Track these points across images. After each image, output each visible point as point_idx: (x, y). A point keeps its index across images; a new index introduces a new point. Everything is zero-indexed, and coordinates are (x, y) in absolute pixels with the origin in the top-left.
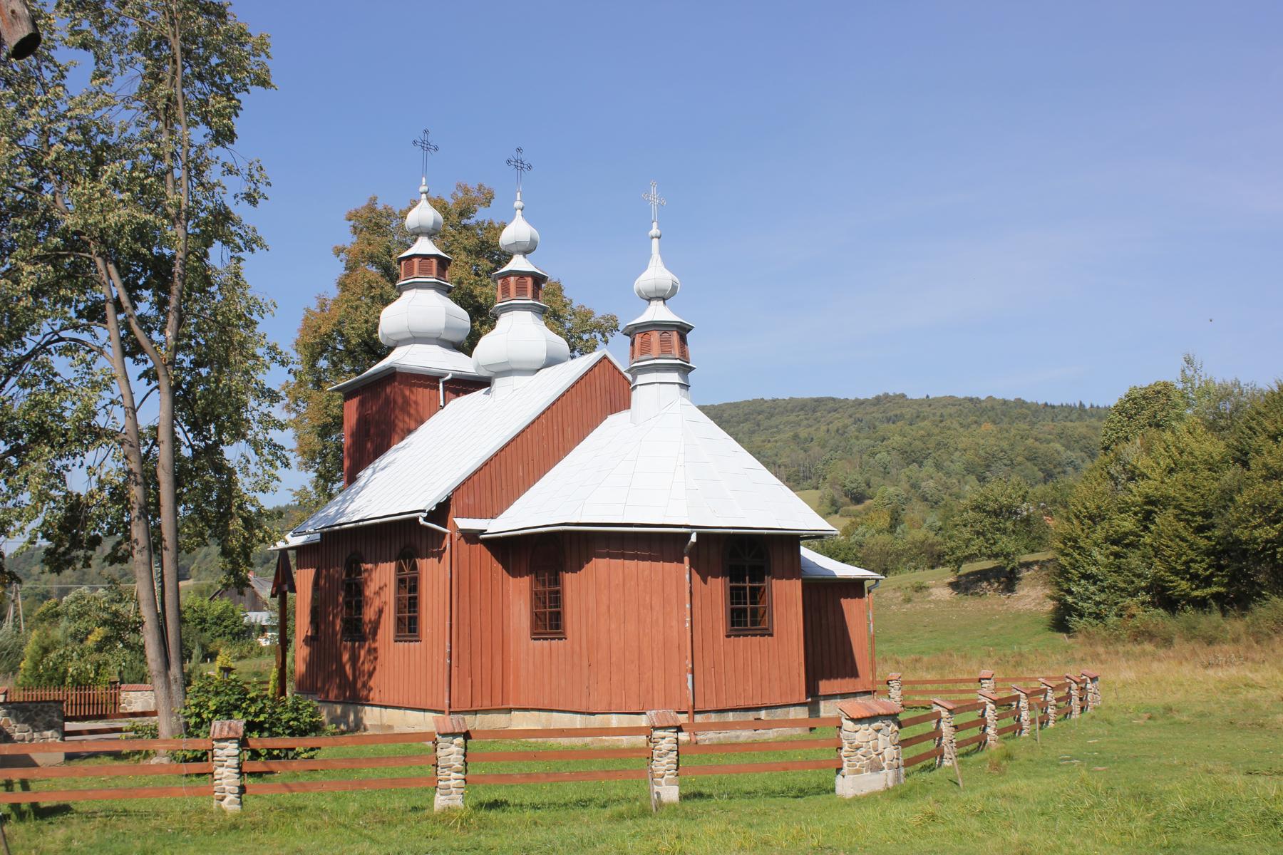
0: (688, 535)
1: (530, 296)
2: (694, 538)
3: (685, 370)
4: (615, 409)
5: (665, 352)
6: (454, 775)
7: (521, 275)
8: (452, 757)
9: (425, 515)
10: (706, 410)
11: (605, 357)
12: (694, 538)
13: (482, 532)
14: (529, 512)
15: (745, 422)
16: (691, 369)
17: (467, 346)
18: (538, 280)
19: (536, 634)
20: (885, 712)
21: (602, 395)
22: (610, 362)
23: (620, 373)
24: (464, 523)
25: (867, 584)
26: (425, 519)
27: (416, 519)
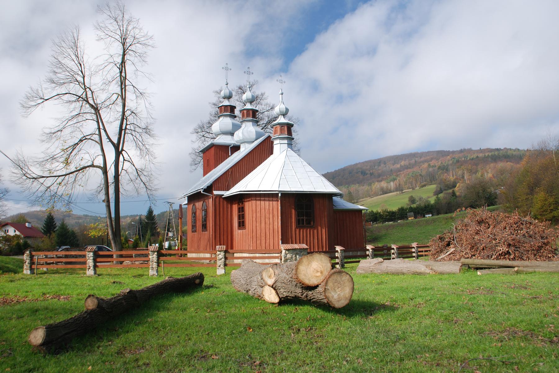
0: (278, 194)
2: (280, 195)
5: (281, 133)
12: (280, 195)
24: (215, 192)
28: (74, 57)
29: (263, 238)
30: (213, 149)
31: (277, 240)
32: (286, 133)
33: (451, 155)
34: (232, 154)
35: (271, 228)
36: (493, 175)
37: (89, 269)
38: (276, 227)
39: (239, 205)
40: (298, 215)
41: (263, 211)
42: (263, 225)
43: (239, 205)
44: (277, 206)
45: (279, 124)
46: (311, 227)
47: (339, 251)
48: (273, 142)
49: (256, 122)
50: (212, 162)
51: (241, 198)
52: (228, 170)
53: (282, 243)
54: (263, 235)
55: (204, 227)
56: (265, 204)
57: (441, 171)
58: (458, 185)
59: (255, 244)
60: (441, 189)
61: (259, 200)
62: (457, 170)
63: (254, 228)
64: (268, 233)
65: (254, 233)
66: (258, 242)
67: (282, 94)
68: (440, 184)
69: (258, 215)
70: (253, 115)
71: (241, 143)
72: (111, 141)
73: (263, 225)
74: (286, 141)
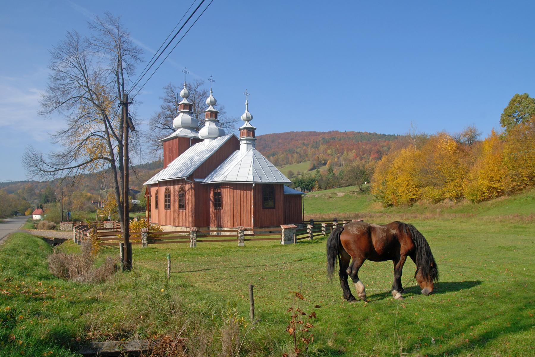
21: (232, 145)
24: (197, 180)
28: (76, 64)
29: (239, 217)
30: (177, 139)
32: (252, 135)
33: (321, 136)
38: (249, 209)
42: (239, 207)
56: (240, 193)
58: (328, 162)
60: (314, 165)
63: (232, 209)
66: (235, 219)
69: (235, 199)
73: (239, 207)
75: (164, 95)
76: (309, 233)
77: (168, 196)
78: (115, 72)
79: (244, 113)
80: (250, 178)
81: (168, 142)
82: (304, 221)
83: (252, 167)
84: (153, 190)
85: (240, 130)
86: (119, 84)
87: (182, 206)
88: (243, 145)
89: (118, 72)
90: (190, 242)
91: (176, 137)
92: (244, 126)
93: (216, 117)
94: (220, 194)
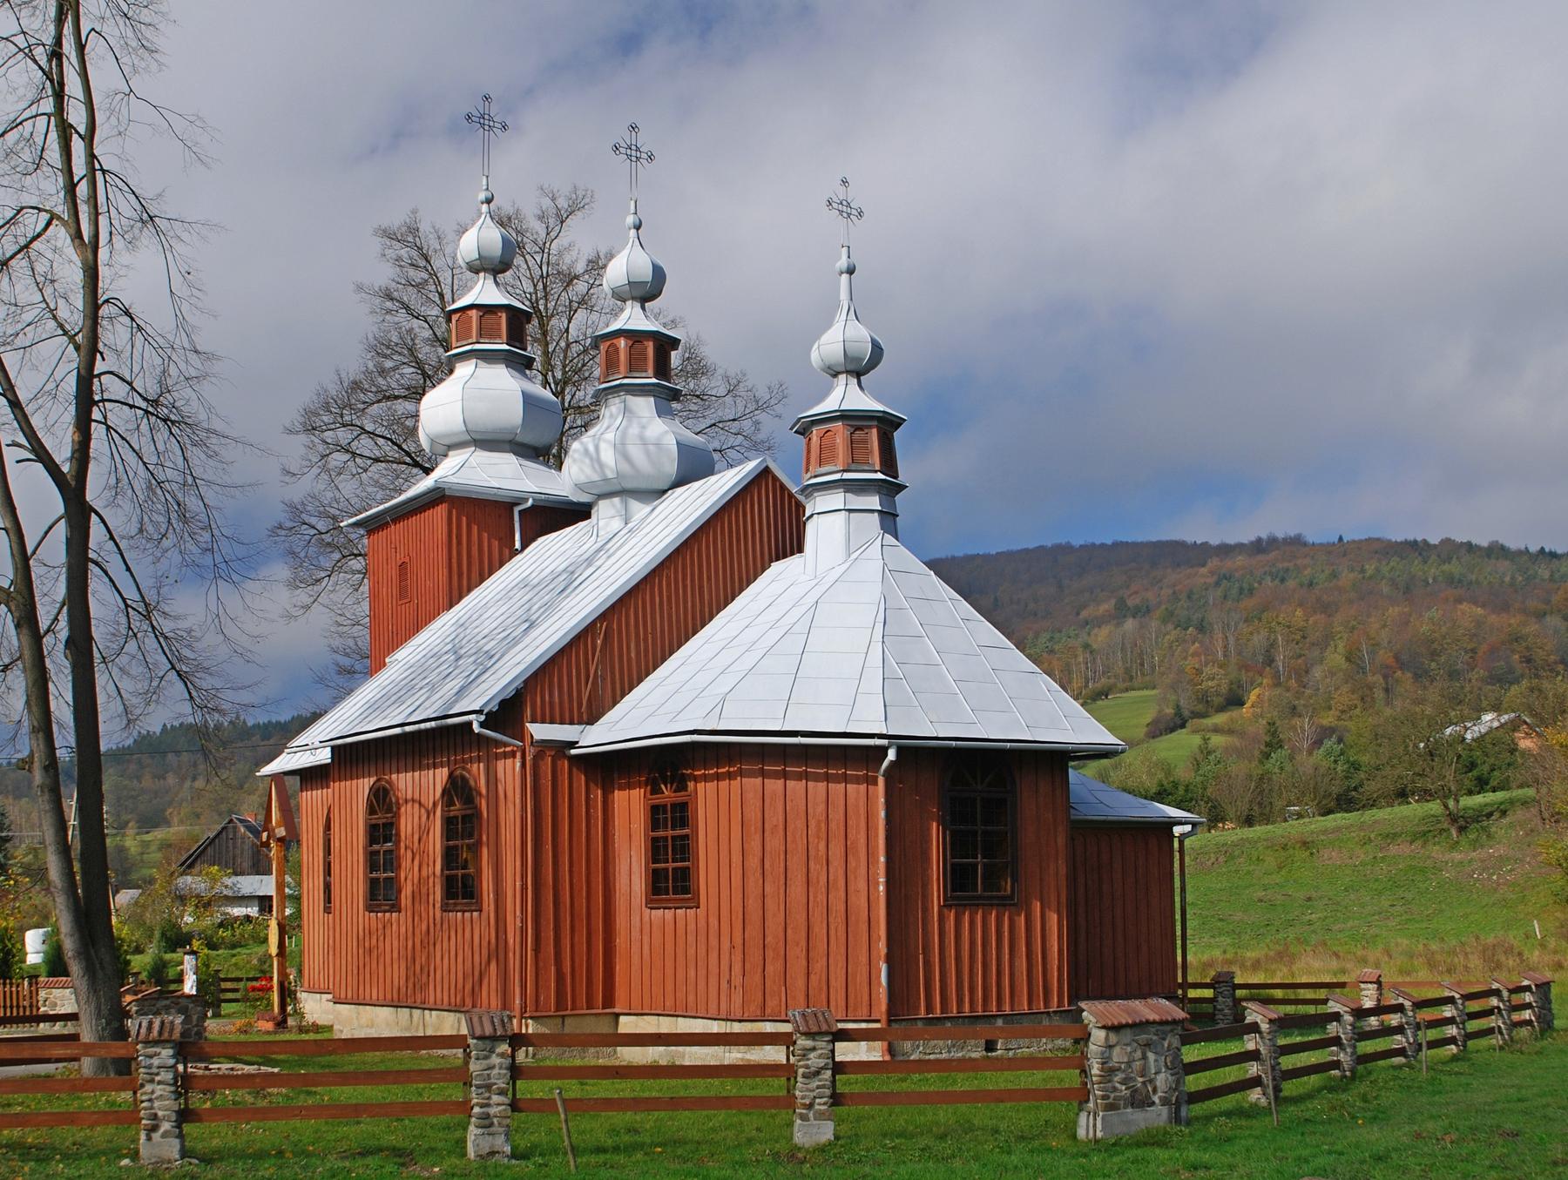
0: (883, 751)
1: (650, 372)
2: (892, 755)
3: (889, 489)
4: (781, 554)
5: (854, 463)
6: (496, 1098)
7: (635, 336)
8: (496, 1071)
9: (482, 718)
10: (943, 568)
11: (765, 473)
12: (892, 755)
13: (573, 745)
14: (648, 713)
15: (998, 586)
16: (902, 487)
17: (548, 453)
18: (665, 344)
19: (370, 908)
20: (1157, 1018)
21: (760, 527)
22: (775, 479)
23: (791, 496)
24: (540, 731)
25: (1177, 830)
26: (482, 725)
27: (470, 724)
29: (797, 953)
30: (441, 511)
31: (864, 959)
33: (1213, 563)
34: (524, 546)
35: (838, 906)
36: (1397, 658)
37: (154, 1128)
39: (656, 790)
40: (959, 844)
41: (797, 824)
43: (656, 790)
44: (870, 801)
45: (844, 416)
46: (1005, 903)
47: (1264, 1027)
48: (800, 508)
49: (667, 398)
50: (434, 574)
51: (669, 765)
52: (594, 623)
53: (270, 898)
54: (797, 935)
55: (460, 889)
56: (808, 794)
57: (1174, 634)
58: (1253, 697)
59: (758, 978)
61: (775, 775)
62: (1245, 629)
63: (753, 904)
64: (819, 930)
65: (753, 931)
67: (851, 271)
68: (1174, 687)
69: (774, 843)
70: (657, 363)
71: (601, 496)
72: (42, 455)
74: (874, 502)
75: (384, 274)
76: (1528, 1006)
77: (381, 831)
78: (40, 53)
79: (829, 325)
80: (864, 716)
81: (396, 530)
82: (1186, 985)
83: (877, 649)
84: (313, 801)
85: (804, 429)
86: (65, 131)
87: (460, 889)
88: (832, 525)
89: (56, 54)
90: (1082, 1095)
91: (438, 497)
92: (830, 404)
93: (662, 369)
94: (682, 814)
